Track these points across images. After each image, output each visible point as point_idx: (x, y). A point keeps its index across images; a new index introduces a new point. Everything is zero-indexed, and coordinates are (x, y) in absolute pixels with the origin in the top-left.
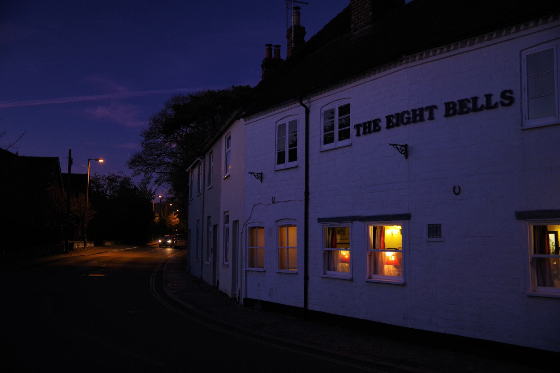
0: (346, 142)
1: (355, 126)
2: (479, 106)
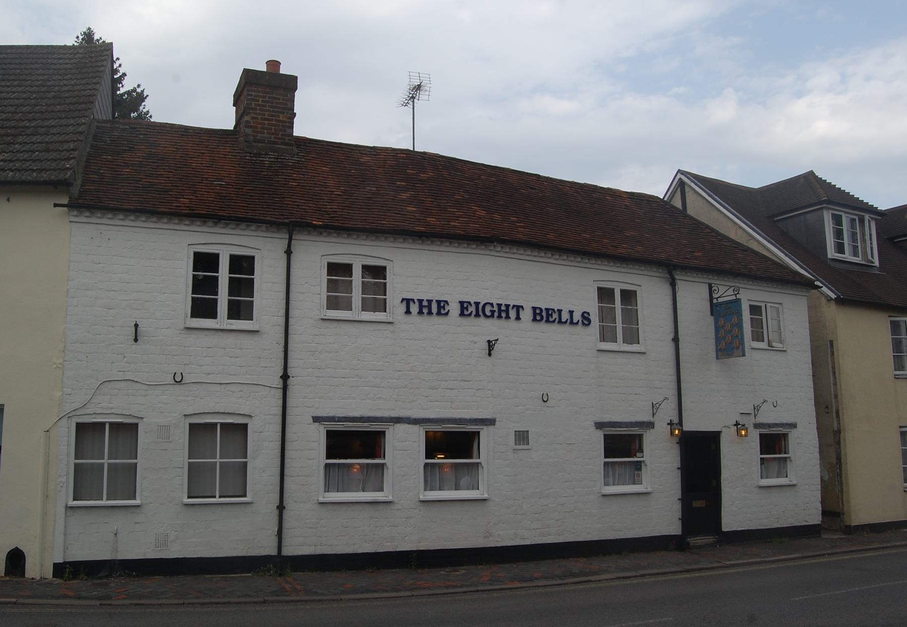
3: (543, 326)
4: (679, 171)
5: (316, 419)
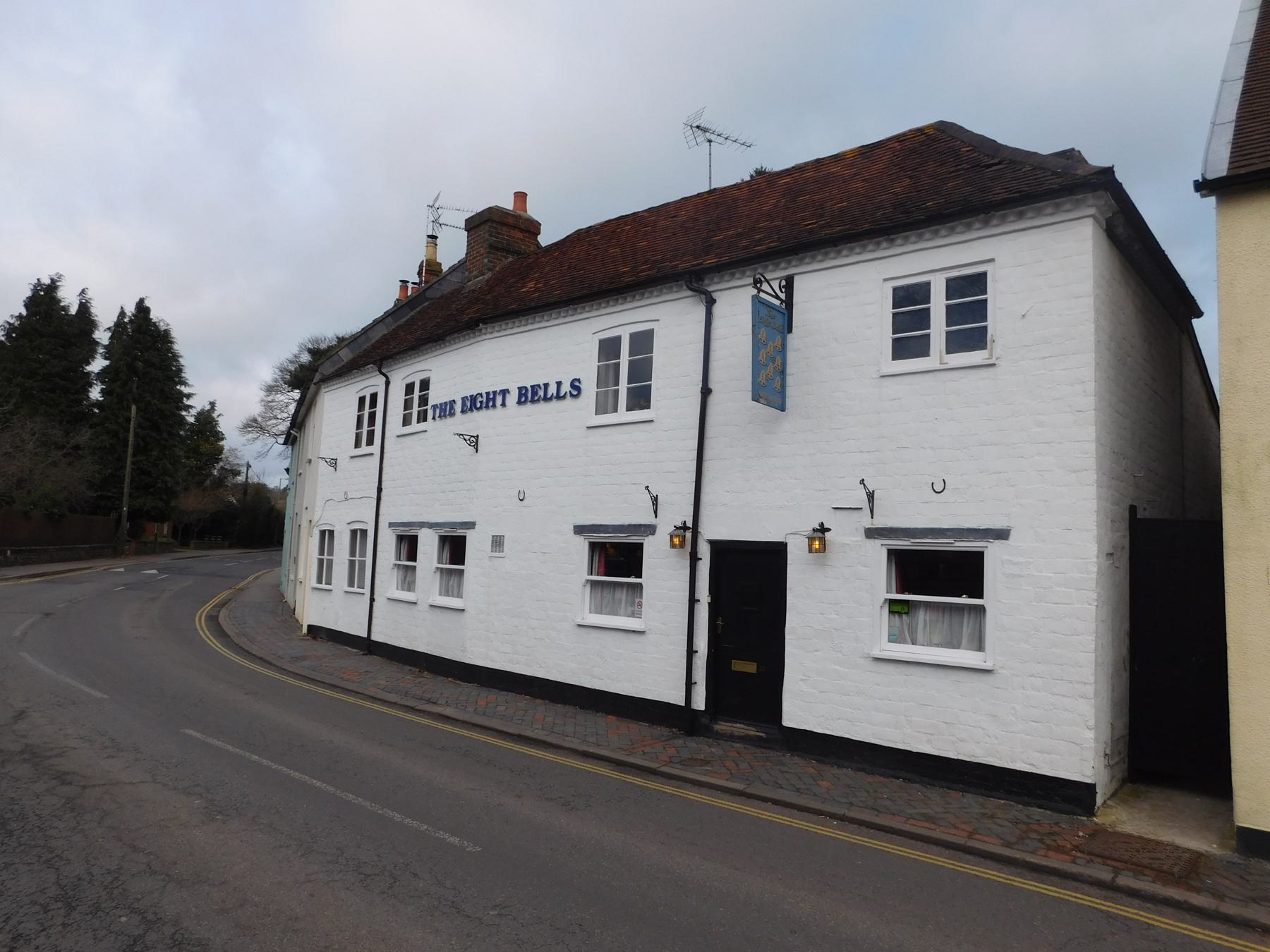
0: (422, 426)
1: (432, 406)
2: (549, 395)
3: (529, 408)
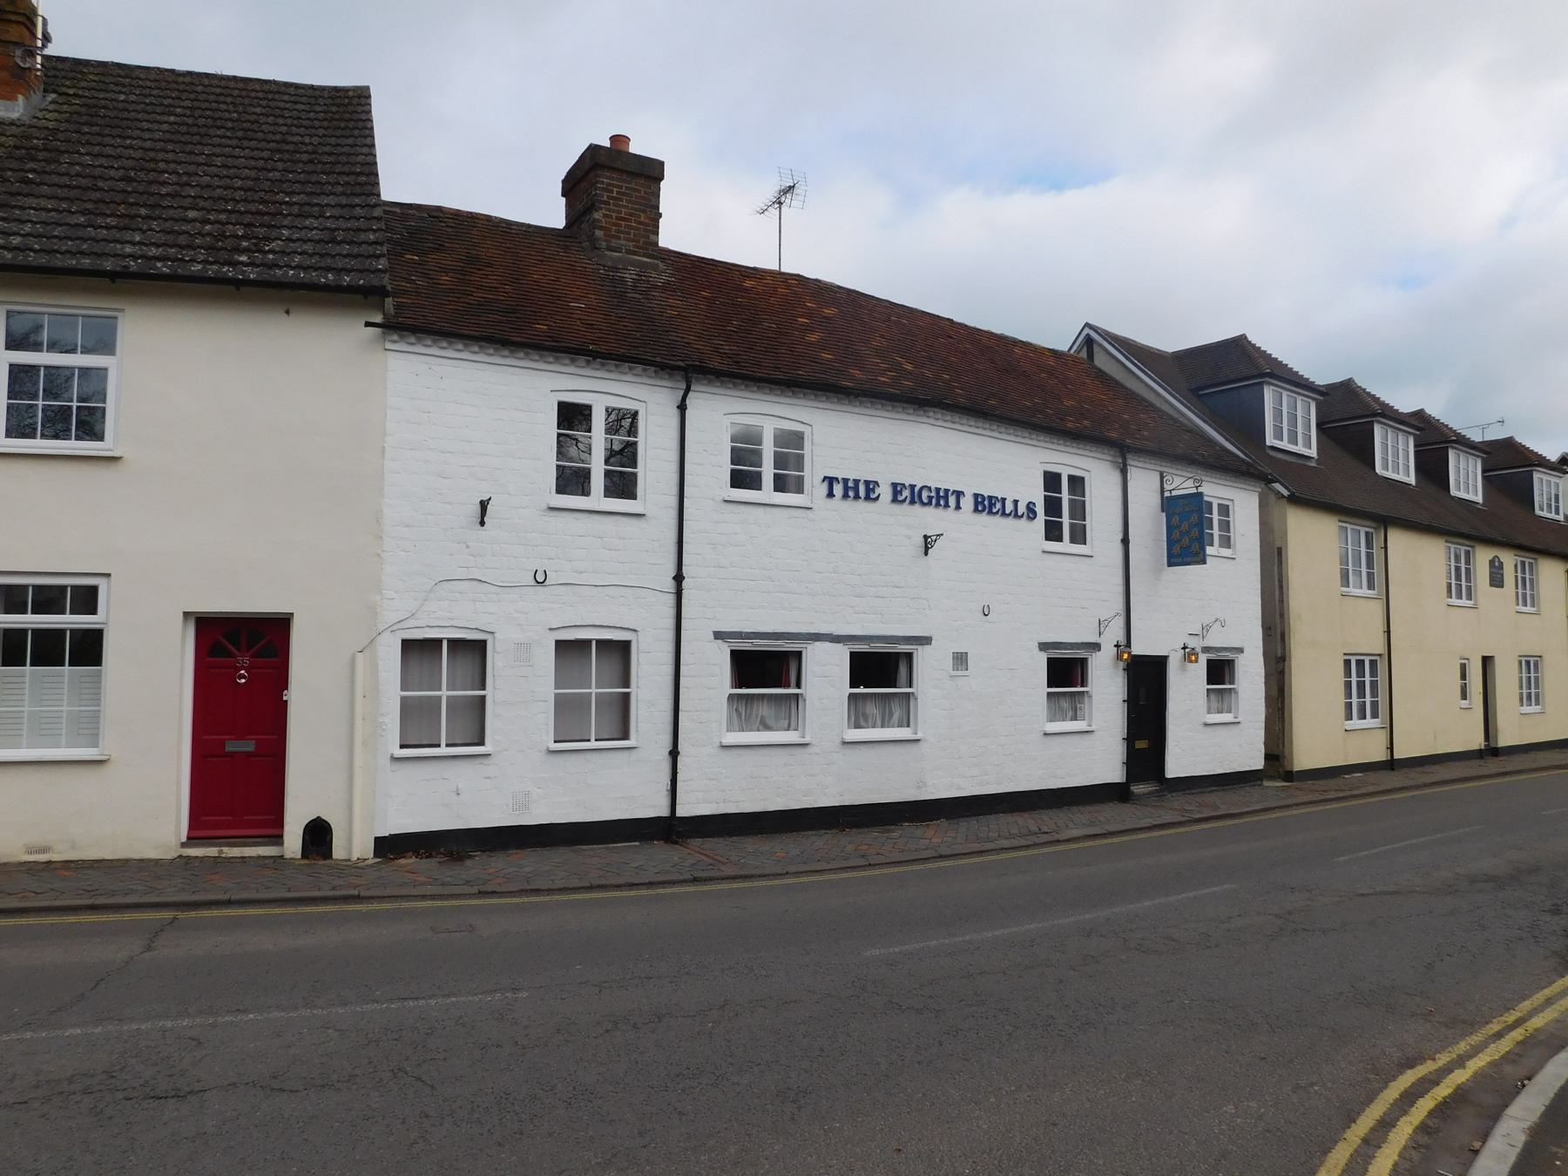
3: (984, 518)
4: (1087, 325)
5: (719, 635)
